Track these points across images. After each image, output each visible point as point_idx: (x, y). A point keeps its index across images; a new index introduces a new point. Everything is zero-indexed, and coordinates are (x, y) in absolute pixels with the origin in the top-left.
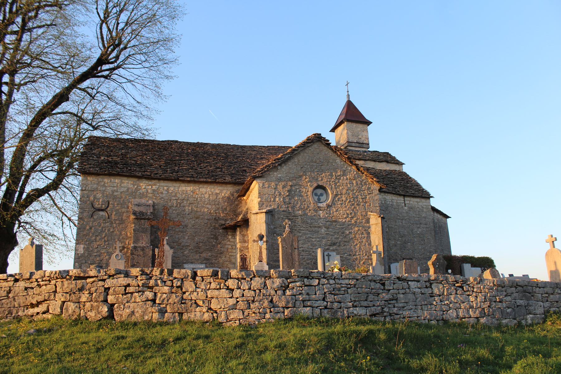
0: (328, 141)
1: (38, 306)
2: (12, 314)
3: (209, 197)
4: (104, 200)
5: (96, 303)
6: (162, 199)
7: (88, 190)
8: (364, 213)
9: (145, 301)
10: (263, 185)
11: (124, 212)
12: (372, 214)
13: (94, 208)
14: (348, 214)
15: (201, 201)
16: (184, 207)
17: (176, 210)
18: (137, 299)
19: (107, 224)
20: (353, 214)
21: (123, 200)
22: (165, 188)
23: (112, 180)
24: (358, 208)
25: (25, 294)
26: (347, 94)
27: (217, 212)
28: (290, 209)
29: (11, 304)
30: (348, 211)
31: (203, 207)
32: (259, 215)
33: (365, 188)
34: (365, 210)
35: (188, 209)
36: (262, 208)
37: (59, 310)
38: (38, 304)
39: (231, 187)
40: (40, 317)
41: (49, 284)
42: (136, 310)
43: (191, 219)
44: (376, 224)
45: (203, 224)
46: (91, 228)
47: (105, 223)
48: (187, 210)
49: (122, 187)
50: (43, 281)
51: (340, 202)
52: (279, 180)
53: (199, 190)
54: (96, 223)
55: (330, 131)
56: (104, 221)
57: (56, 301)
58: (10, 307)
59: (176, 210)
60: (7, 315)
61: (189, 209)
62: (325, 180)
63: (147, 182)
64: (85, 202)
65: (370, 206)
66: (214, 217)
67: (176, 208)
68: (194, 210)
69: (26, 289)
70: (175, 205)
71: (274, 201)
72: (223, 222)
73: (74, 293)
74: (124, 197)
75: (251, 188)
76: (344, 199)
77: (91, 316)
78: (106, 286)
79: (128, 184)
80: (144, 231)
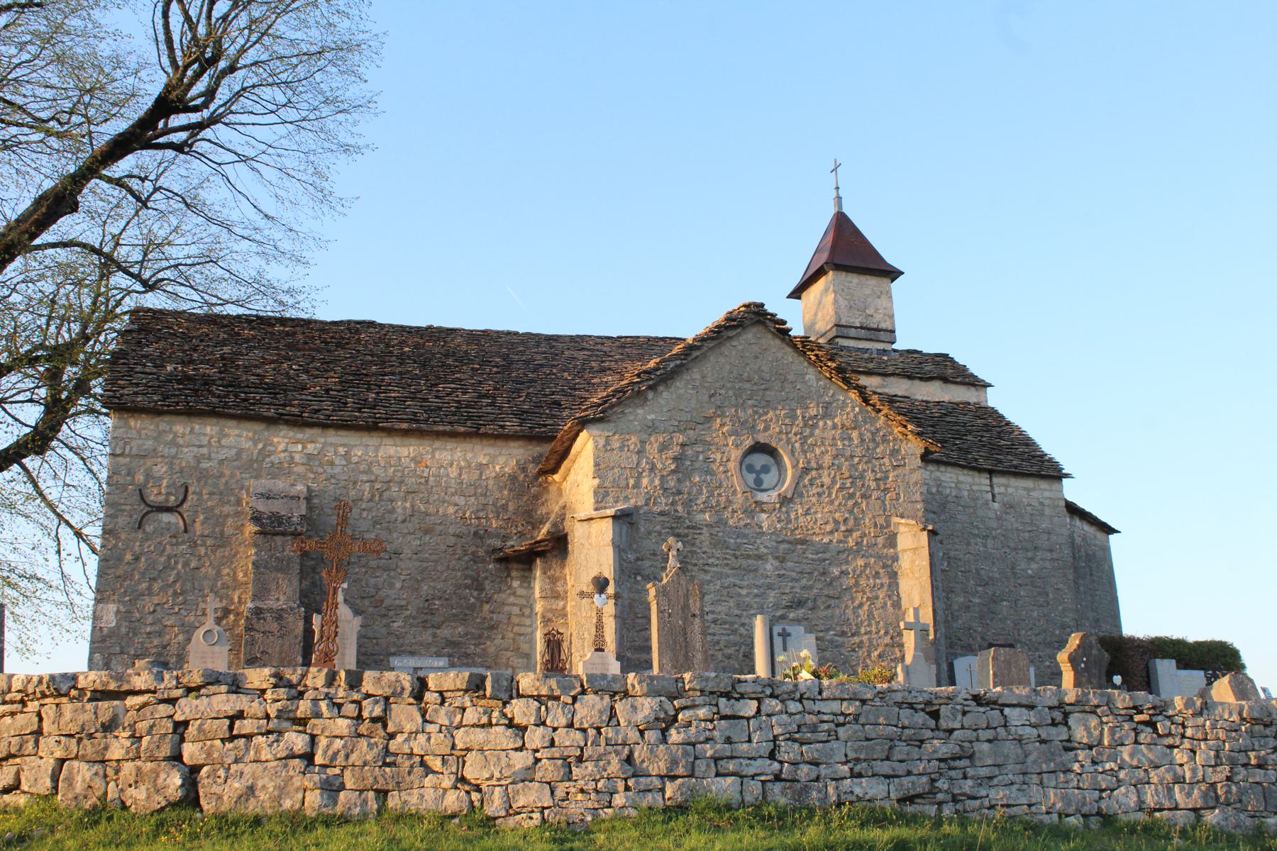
0: (784, 323)
3: (460, 475)
4: (174, 483)
5: (149, 764)
6: (333, 481)
8: (881, 521)
10: (607, 442)
11: (228, 516)
13: (149, 506)
14: (836, 522)
15: (438, 484)
18: (263, 752)
23: (197, 427)
26: (834, 194)
27: (481, 514)
28: (680, 508)
30: (837, 515)
31: (444, 502)
32: (595, 525)
37: (48, 783)
39: (520, 447)
41: (22, 712)
42: (260, 783)
43: (409, 533)
45: (444, 548)
46: (137, 559)
47: (177, 544)
48: (400, 510)
51: (814, 490)
53: (433, 457)
54: (150, 546)
55: (789, 297)
56: (174, 540)
57: (41, 758)
59: (370, 510)
61: (405, 508)
63: (291, 434)
64: (123, 488)
65: (897, 499)
66: (472, 530)
67: (371, 504)
70: (367, 495)
72: (498, 544)
73: (91, 736)
74: (228, 473)
75: (573, 451)
77: (136, 799)
78: (179, 717)
79: (238, 439)
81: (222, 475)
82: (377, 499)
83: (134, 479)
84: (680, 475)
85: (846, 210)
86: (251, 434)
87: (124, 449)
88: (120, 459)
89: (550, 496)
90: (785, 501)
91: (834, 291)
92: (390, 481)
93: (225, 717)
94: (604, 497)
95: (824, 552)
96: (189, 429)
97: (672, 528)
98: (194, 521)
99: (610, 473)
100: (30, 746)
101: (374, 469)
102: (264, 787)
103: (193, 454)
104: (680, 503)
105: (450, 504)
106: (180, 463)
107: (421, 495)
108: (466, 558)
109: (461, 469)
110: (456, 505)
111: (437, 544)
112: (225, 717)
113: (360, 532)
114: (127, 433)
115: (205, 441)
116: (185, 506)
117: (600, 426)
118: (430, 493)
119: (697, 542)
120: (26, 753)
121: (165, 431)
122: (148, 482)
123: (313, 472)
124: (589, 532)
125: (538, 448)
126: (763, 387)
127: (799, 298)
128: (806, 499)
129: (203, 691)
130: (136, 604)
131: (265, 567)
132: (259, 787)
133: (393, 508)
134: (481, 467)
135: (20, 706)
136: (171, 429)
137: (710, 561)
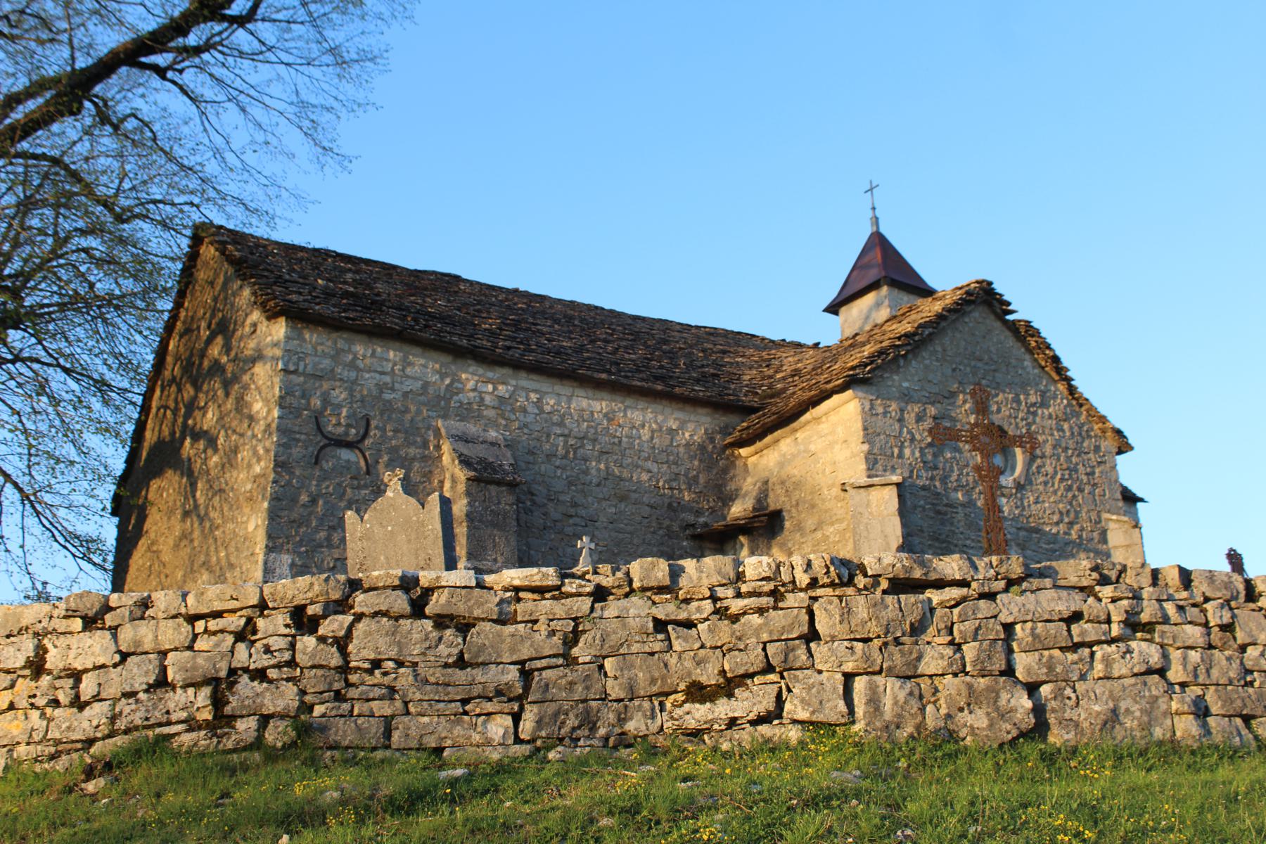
0: (1009, 304)
1: (730, 695)
2: (593, 729)
3: (652, 438)
4: (355, 414)
5: (981, 680)
6: (526, 431)
7: (304, 374)
8: (1093, 516)
9: (1142, 674)
10: (872, 408)
11: (414, 459)
12: (1114, 517)
13: (326, 437)
14: (1061, 513)
15: (631, 447)
16: (585, 460)
17: (564, 468)
18: (1116, 666)
19: (363, 492)
20: (1072, 515)
21: (412, 420)
22: (534, 397)
23: (379, 350)
24: (1080, 498)
25: (657, 646)
26: (870, 214)
27: (674, 484)
28: (937, 484)
29: (587, 688)
30: (1061, 506)
31: (637, 466)
32: (875, 494)
33: (1089, 447)
34: (1096, 505)
35: (597, 467)
36: (873, 472)
37: (842, 706)
38: (729, 686)
39: (707, 415)
40: (745, 735)
41: (775, 608)
42: (1123, 705)
43: (604, 499)
44: (1128, 546)
45: (638, 518)
46: (314, 501)
47: (359, 488)
48: (593, 472)
49: (408, 377)
50: (739, 595)
51: (1041, 479)
52: (906, 397)
53: (625, 415)
54: (328, 487)
55: (825, 310)
56: (355, 482)
57: (820, 672)
58: (585, 701)
59: (564, 468)
60: (574, 729)
61: (599, 470)
62: (1005, 412)
63: (481, 371)
64: (296, 412)
65: (1104, 495)
66: (667, 501)
67: (564, 461)
68: (614, 475)
69: (660, 626)
70: (561, 451)
71: (901, 456)
72: (691, 518)
73: (897, 641)
74: (413, 408)
75: (803, 419)
76: (1050, 469)
77: (972, 727)
78: (1005, 618)
79: (424, 370)
80: (498, 523)
81: (407, 411)
82: (571, 455)
83: (309, 403)
84: (935, 449)
85: (883, 230)
86: (437, 366)
87: (298, 365)
88: (292, 377)
89: (737, 472)
90: (1019, 487)
91: (889, 306)
92: (583, 438)
93: (1061, 620)
94: (874, 464)
95: (1054, 543)
96: (370, 351)
97: (933, 504)
98: (377, 462)
99: (877, 439)
100: (801, 654)
101: (567, 422)
102: (1127, 710)
103: (375, 382)
104: (938, 478)
105: (643, 469)
106: (361, 391)
107: (615, 457)
108: (661, 532)
109: (653, 431)
110: (649, 471)
111: (632, 514)
112: (1061, 620)
113: (555, 492)
114: (301, 346)
115: (388, 367)
116: (366, 442)
117: (865, 388)
118: (623, 455)
119: (955, 521)
120: (798, 665)
121: (343, 350)
122: (326, 409)
123: (506, 419)
124: (868, 501)
125: (724, 418)
126: (993, 367)
127: (836, 313)
128: (1034, 487)
129: (1025, 585)
130: (313, 557)
131: (480, 521)
132: (1122, 710)
133: (588, 468)
134: (671, 432)
135: (771, 600)
136: (350, 348)
137: (968, 542)
